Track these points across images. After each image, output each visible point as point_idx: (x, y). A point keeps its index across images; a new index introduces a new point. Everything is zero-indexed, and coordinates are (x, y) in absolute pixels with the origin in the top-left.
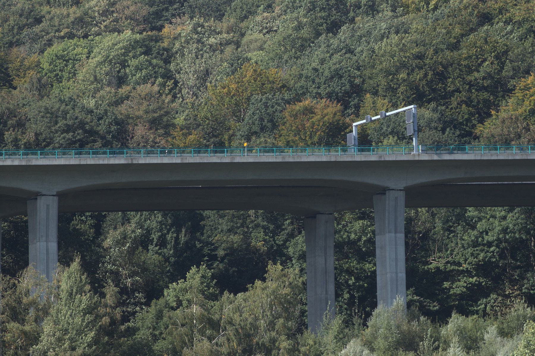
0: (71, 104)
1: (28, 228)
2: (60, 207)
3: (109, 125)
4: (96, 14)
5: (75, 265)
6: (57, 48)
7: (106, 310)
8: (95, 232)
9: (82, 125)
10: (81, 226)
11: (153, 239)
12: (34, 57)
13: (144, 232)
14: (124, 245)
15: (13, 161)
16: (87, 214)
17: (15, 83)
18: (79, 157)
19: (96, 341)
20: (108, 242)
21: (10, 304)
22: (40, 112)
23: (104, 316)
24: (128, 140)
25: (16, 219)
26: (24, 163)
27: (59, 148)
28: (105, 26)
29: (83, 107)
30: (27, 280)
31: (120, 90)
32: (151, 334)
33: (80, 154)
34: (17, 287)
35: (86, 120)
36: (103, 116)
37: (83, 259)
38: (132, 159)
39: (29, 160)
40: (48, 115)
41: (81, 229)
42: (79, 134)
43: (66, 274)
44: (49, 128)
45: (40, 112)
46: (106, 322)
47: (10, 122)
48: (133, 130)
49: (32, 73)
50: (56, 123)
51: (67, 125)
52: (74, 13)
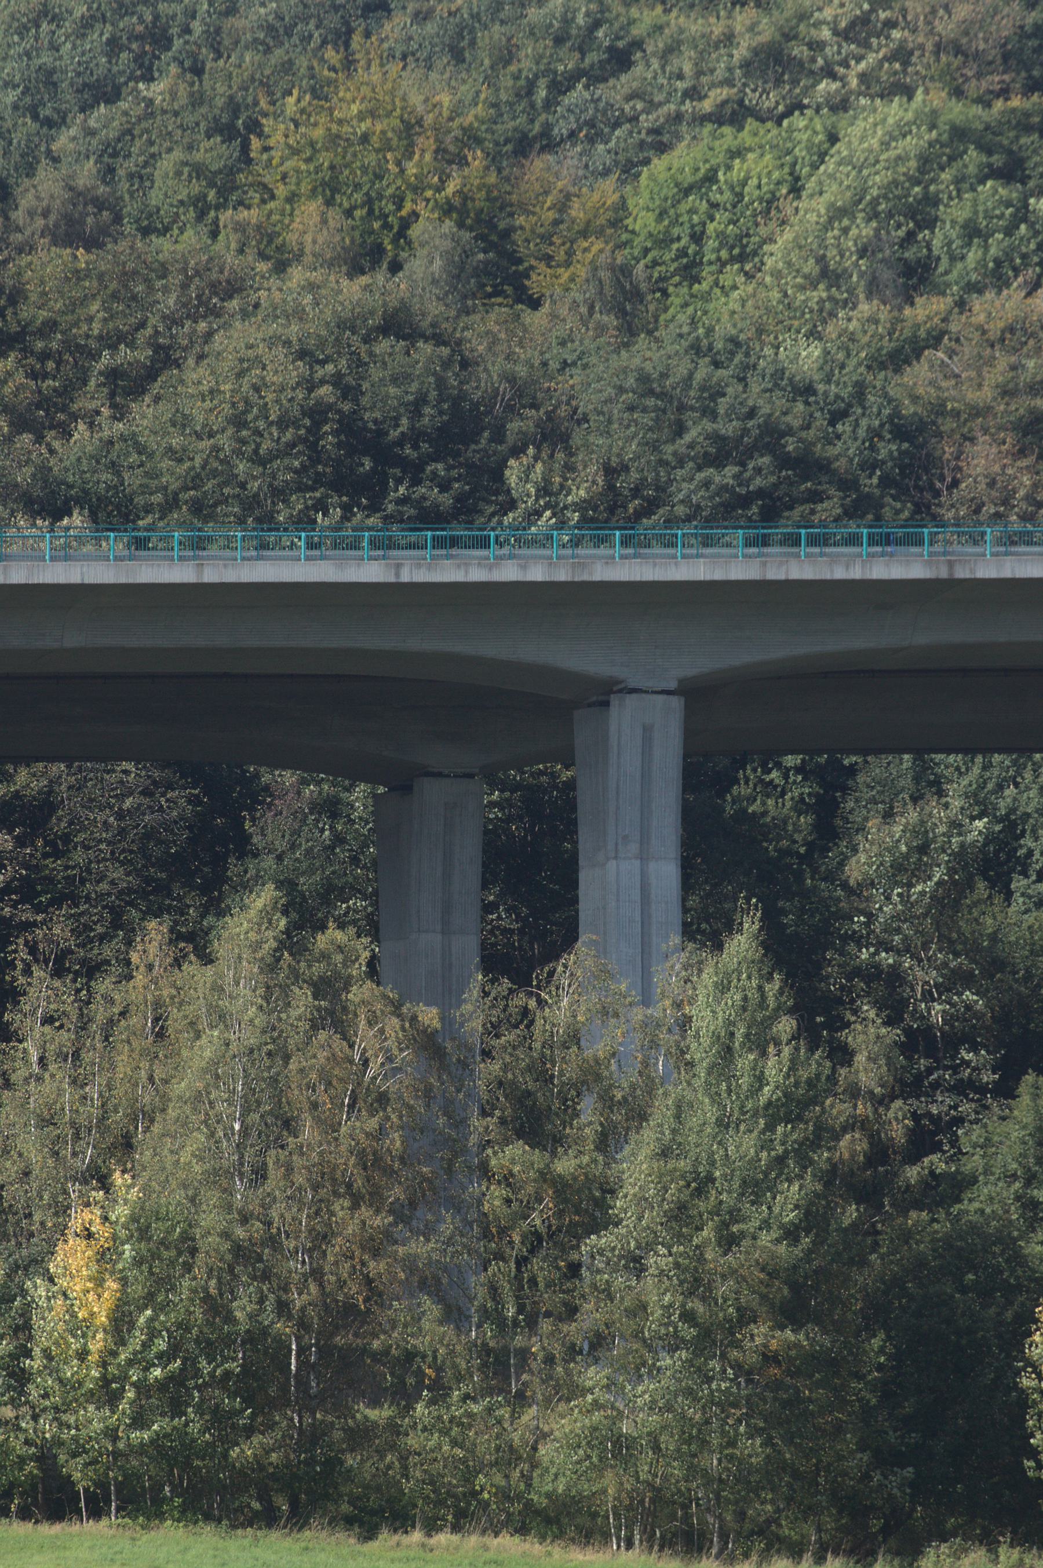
0: (736, 360)
1: (574, 808)
2: (689, 734)
3: (871, 440)
4: (826, 33)
5: (742, 944)
6: (684, 158)
7: (855, 1106)
8: (816, 827)
9: (771, 436)
10: (764, 803)
11: (1030, 853)
12: (607, 190)
13: (998, 828)
14: (921, 872)
15: (524, 568)
16: (791, 760)
17: (535, 284)
18: (759, 555)
19: (814, 1218)
20: (858, 867)
21: (513, 1082)
22: (621, 390)
23: (845, 1129)
24: (937, 494)
25: (532, 774)
26: (562, 575)
27: (688, 519)
28: (863, 77)
29: (779, 373)
30: (567, 1000)
31: (907, 311)
32: (1018, 1198)
33: (765, 544)
34: (532, 1022)
35: (788, 419)
36: (850, 405)
37: (770, 921)
38: (951, 564)
39: (582, 566)
40: (651, 402)
41: (765, 813)
42: (762, 472)
43: (709, 977)
44: (655, 447)
45: (621, 390)
46: (853, 1154)
47: (514, 426)
48: (958, 458)
49: (594, 249)
50: (680, 430)
51: (716, 438)
52: (752, 29)
